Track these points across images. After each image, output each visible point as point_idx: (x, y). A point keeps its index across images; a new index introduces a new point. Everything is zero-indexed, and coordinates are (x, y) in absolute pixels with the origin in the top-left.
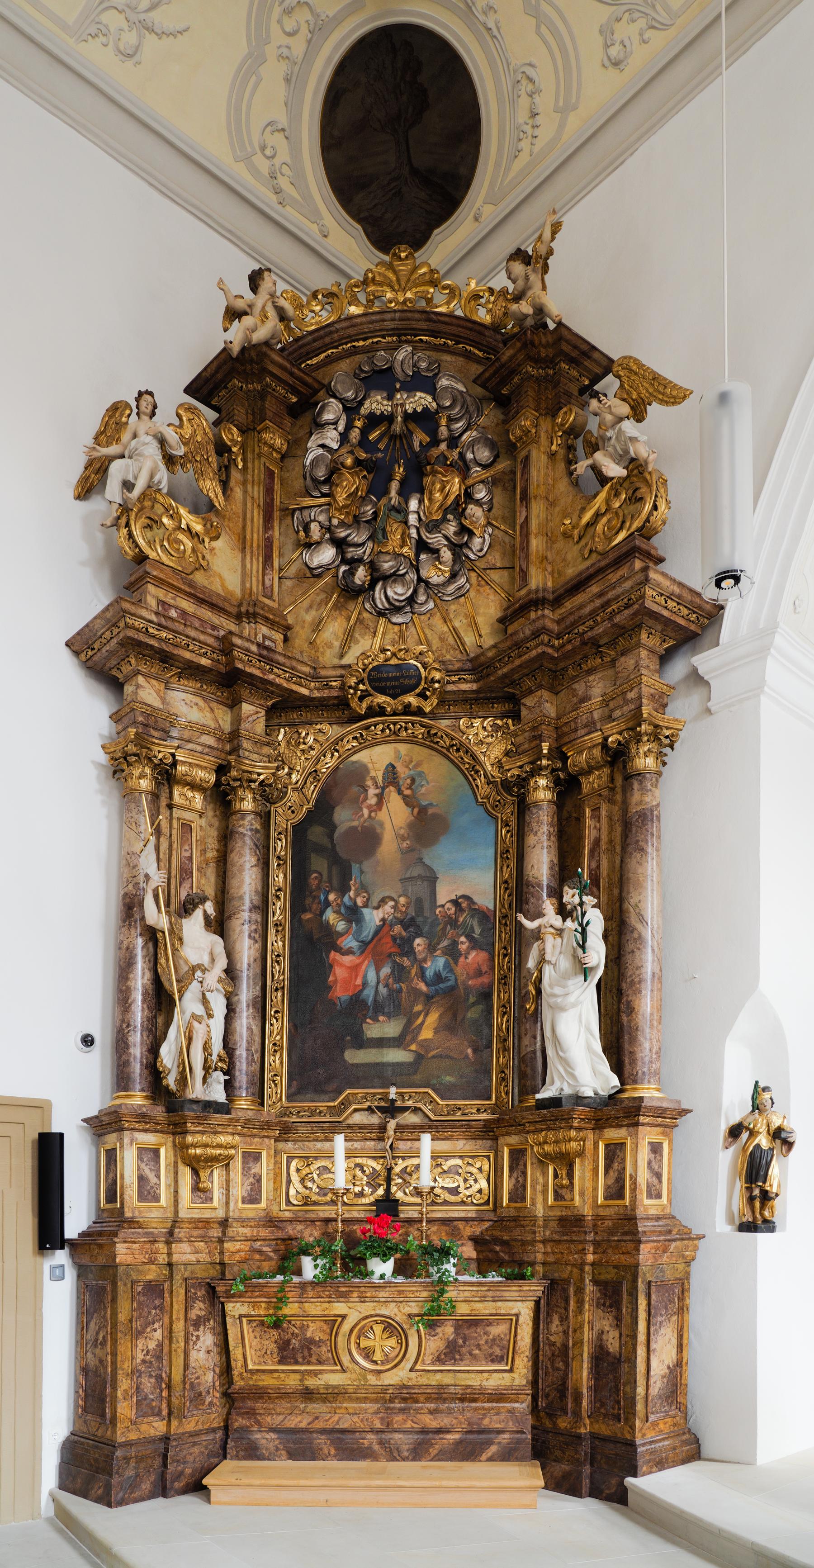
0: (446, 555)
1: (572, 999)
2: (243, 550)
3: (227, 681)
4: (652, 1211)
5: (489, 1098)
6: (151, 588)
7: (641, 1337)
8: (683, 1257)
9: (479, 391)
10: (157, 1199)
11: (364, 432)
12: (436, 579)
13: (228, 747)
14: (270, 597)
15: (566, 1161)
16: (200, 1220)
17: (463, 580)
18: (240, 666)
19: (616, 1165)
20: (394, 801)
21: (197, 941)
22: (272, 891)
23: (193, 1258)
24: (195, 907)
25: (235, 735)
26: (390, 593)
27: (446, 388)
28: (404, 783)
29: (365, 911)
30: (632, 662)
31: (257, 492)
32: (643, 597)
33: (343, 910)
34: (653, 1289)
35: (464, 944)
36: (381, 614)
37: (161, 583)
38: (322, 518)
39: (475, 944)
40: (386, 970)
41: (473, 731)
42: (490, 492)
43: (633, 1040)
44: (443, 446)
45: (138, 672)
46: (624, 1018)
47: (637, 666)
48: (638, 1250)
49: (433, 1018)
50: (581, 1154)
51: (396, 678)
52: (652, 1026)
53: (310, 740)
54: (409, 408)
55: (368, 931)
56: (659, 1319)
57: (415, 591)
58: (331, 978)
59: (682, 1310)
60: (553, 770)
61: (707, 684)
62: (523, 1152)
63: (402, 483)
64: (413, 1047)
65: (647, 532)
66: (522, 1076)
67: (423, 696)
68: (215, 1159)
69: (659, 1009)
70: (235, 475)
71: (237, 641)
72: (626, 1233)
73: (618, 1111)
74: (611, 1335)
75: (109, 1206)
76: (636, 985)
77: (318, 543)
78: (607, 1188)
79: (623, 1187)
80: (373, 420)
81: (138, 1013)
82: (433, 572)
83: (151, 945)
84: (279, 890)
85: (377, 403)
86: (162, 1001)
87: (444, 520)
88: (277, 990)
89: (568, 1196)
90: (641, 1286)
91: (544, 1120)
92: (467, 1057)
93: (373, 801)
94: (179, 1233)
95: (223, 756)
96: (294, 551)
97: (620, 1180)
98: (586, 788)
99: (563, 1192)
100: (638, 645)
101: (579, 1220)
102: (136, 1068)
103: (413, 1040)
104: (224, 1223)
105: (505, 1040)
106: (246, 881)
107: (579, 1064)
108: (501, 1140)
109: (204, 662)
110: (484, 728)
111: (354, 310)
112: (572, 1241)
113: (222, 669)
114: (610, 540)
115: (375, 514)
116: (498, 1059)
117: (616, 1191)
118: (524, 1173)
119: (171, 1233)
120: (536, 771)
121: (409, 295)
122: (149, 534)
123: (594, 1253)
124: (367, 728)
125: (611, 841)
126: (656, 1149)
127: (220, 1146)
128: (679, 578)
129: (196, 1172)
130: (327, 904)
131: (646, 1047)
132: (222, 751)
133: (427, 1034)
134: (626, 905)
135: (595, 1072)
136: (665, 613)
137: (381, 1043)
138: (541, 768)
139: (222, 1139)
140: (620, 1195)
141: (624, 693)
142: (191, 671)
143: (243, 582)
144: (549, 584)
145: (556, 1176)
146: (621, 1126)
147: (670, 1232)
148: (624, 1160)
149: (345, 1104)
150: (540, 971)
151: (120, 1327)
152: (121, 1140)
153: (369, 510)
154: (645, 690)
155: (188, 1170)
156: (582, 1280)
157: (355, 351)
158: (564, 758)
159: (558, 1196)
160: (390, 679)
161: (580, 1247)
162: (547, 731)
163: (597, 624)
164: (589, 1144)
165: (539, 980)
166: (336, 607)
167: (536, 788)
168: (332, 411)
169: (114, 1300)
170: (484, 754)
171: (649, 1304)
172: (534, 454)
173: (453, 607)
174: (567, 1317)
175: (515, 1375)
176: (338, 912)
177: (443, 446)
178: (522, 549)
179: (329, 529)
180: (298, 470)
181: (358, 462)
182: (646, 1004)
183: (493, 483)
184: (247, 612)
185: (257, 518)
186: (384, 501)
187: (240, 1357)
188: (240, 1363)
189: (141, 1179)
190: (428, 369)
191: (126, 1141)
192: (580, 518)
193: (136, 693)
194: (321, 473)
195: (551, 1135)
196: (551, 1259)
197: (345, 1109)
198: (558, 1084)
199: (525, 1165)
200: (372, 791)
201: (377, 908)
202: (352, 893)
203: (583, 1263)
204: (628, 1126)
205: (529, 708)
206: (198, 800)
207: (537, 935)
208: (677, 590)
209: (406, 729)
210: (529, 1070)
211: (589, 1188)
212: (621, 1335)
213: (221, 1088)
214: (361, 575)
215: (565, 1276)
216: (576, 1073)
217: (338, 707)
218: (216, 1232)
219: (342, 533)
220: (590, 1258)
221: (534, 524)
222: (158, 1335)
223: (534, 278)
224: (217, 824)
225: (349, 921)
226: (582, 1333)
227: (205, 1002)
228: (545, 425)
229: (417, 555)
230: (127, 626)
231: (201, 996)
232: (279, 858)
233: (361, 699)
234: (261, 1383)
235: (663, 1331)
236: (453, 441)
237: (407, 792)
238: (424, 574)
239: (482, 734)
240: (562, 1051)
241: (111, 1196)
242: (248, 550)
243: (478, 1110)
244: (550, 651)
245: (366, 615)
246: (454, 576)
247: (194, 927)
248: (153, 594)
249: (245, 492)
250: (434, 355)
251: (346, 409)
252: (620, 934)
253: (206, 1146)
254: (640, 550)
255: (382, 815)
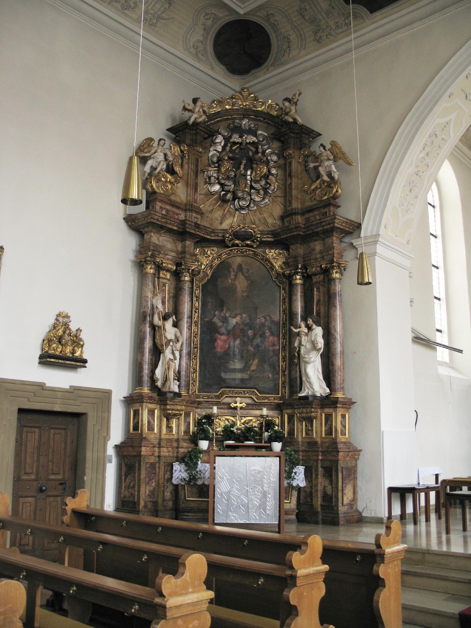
0: (262, 192)
1: (312, 360)
2: (187, 186)
3: (182, 233)
4: (343, 440)
5: (279, 394)
6: (158, 203)
7: (340, 488)
8: (354, 458)
9: (272, 136)
10: (153, 430)
11: (231, 147)
12: (257, 199)
13: (180, 256)
14: (196, 203)
15: (310, 420)
16: (169, 439)
17: (267, 200)
18: (188, 230)
19: (329, 423)
20: (241, 277)
21: (170, 331)
22: (194, 309)
23: (167, 454)
24: (170, 317)
25: (183, 252)
26: (240, 203)
27: (261, 134)
28: (245, 271)
29: (229, 319)
30: (331, 241)
31: (193, 167)
32: (334, 223)
33: (221, 318)
34: (344, 470)
35: (268, 333)
36: (236, 210)
37: (161, 201)
38: (215, 175)
39: (272, 334)
40: (238, 342)
41: (271, 254)
42: (277, 171)
43: (334, 376)
44: (260, 155)
45: (152, 232)
46: (331, 367)
47: (332, 243)
48: (338, 455)
49: (256, 361)
50: (316, 418)
51: (244, 236)
52: (340, 371)
53: (209, 252)
54: (248, 141)
55: (230, 327)
56: (346, 481)
57: (250, 203)
58: (216, 344)
59: (355, 479)
60: (302, 273)
61: (357, 249)
62: (293, 416)
63: (245, 165)
64: (248, 373)
65: (335, 197)
66: (291, 387)
67: (253, 241)
68: (175, 415)
69: (343, 364)
70: (185, 161)
71: (188, 222)
72: (333, 448)
73: (329, 402)
74: (328, 488)
75: (135, 432)
76: (334, 355)
77: (214, 184)
78: (326, 431)
79: (332, 431)
80: (234, 143)
81: (147, 356)
82: (256, 197)
83: (153, 331)
84: (197, 309)
85: (236, 138)
86: (157, 352)
87: (261, 180)
88: (195, 348)
89: (311, 434)
90: (340, 468)
91: (302, 405)
92: (269, 377)
93: (233, 277)
94: (163, 444)
95: (178, 259)
96: (204, 185)
97: (331, 428)
98: (314, 280)
99: (309, 432)
100: (333, 236)
101: (316, 443)
102: (146, 378)
103: (248, 370)
104: (177, 440)
105: (285, 372)
106: (186, 308)
107: (315, 383)
108: (284, 411)
109: (175, 228)
110: (275, 253)
111: (227, 107)
112: (313, 451)
113: (181, 230)
114: (322, 198)
115: (235, 176)
116: (282, 379)
117: (329, 432)
118: (294, 424)
119: (159, 444)
120: (297, 273)
121: (247, 103)
122: (158, 184)
123: (322, 456)
124: (231, 250)
125: (324, 301)
126: (343, 416)
127: (178, 410)
128: (345, 217)
129: (168, 420)
130: (215, 315)
131: (338, 378)
132: (178, 258)
133: (253, 368)
134: (330, 326)
135: (321, 387)
136: (342, 227)
137: (234, 371)
138: (298, 272)
139: (179, 408)
140: (331, 434)
141: (328, 251)
142: (170, 231)
143: (187, 198)
144: (299, 207)
145: (306, 426)
146: (331, 408)
147: (349, 448)
148: (332, 421)
149: (222, 394)
150: (299, 348)
151: (142, 481)
152: (142, 406)
153: (233, 174)
154: (336, 252)
155: (165, 419)
156: (317, 466)
157: (227, 119)
158: (307, 269)
159: (307, 434)
160: (242, 236)
161: (316, 453)
162: (300, 259)
163: (318, 227)
164: (319, 414)
165: (299, 351)
166: (220, 206)
167: (296, 279)
168: (219, 139)
169: (139, 469)
170: (275, 262)
171: (342, 476)
172: (293, 162)
173: (264, 209)
174: (312, 481)
175: (291, 504)
176: (219, 319)
177: (260, 155)
178: (289, 193)
179: (218, 179)
180: (206, 157)
181: (229, 158)
182: (338, 362)
183: (278, 167)
184: (189, 207)
185: (192, 175)
186: (238, 172)
187: (183, 494)
188: (183, 497)
189: (149, 422)
190: (254, 127)
191: (144, 407)
192: (310, 187)
193: (150, 239)
194: (215, 160)
195: (305, 410)
196: (305, 458)
197: (222, 396)
198: (307, 390)
199: (294, 421)
200: (232, 273)
201: (234, 318)
202: (224, 312)
203: (318, 460)
204: (333, 408)
205: (293, 250)
206: (168, 276)
207: (298, 334)
208: (345, 220)
209: (246, 252)
210: (294, 384)
211: (319, 430)
212: (332, 487)
213: (177, 387)
214: (229, 196)
215: (310, 465)
216: (314, 387)
217: (222, 243)
218: (175, 444)
219: (223, 182)
220: (320, 458)
221: (294, 185)
222: (154, 484)
223: (293, 108)
224: (173, 283)
225: (223, 322)
226: (318, 487)
227: (173, 353)
228: (297, 153)
229: (250, 191)
230: (151, 218)
231: (171, 351)
232: (197, 297)
233: (230, 241)
234: (191, 506)
235: (348, 486)
236: (264, 152)
237: (246, 275)
238: (253, 197)
239: (275, 255)
240: (308, 378)
241: (136, 428)
242: (189, 187)
243: (274, 399)
244: (301, 233)
245: (231, 210)
246: (264, 199)
247: (169, 325)
248: (158, 205)
249: (189, 166)
250: (256, 123)
251: (224, 138)
252: (328, 336)
253: (173, 410)
254: (332, 203)
255: (237, 283)
